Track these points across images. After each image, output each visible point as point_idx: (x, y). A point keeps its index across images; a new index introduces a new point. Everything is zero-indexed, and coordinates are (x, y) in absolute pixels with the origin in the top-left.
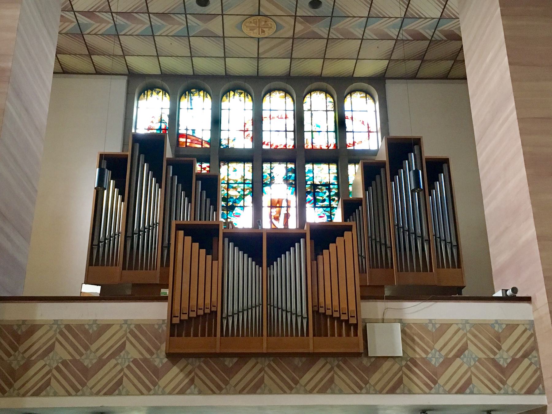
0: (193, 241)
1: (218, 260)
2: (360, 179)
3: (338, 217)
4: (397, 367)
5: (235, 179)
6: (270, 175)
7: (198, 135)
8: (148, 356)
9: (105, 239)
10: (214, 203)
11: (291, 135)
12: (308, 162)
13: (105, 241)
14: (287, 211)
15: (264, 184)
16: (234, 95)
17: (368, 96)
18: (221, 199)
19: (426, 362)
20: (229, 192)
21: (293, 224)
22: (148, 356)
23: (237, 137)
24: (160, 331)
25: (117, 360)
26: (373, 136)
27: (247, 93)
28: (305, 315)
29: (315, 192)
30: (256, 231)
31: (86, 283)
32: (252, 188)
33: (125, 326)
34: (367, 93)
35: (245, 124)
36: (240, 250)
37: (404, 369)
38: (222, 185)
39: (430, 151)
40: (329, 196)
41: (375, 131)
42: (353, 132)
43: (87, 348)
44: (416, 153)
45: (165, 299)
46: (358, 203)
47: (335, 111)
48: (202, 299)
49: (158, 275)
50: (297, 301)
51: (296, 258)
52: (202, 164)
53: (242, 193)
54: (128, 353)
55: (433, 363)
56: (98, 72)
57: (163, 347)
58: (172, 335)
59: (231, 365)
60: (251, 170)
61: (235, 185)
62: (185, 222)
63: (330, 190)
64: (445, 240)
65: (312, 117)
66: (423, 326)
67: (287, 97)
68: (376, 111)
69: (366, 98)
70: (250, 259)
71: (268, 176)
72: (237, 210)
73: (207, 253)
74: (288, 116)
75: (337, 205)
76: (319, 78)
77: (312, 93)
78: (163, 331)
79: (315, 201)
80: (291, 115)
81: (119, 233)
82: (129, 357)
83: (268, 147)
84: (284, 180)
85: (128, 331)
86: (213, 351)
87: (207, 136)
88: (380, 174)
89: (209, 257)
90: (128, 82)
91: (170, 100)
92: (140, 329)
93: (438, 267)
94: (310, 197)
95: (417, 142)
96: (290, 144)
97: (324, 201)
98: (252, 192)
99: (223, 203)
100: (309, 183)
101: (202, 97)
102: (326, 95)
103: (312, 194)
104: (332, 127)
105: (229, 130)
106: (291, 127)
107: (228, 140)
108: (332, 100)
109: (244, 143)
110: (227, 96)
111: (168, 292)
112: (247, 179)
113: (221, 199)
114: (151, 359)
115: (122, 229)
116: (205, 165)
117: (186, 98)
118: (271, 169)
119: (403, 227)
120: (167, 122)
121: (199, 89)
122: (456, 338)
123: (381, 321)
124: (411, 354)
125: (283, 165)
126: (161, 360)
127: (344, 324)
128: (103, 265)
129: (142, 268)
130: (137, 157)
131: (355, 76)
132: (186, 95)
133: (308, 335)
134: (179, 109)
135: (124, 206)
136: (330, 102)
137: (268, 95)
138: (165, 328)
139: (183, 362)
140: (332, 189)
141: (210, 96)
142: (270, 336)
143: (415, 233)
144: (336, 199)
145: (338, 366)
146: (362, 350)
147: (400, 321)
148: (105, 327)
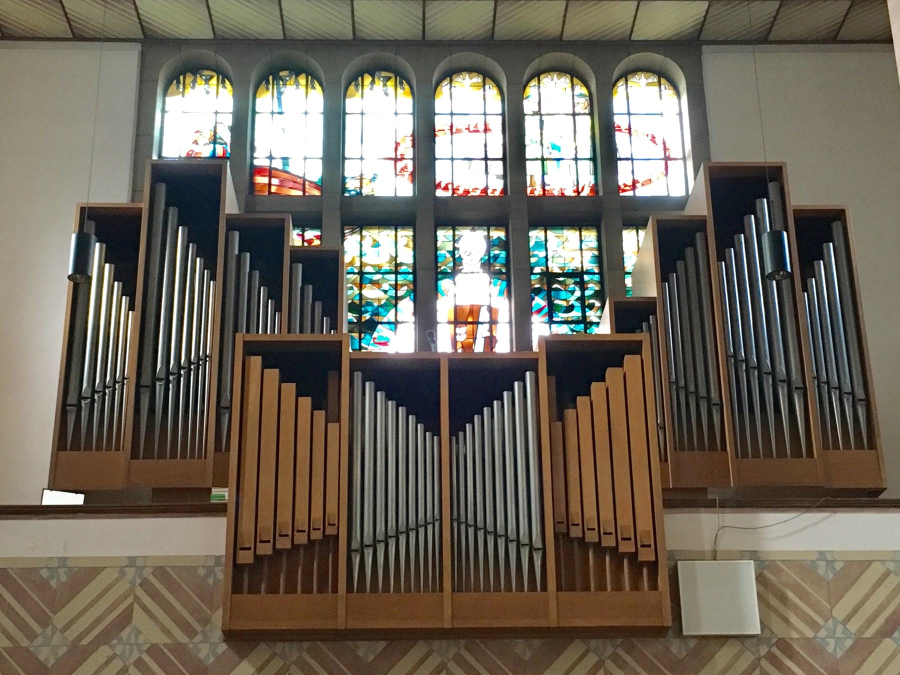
0: (284, 379)
1: (339, 420)
2: (650, 260)
3: (604, 328)
4: (747, 659)
5: (376, 263)
6: (453, 253)
7: (296, 168)
8: (182, 638)
9: (94, 391)
10: (332, 313)
11: (497, 168)
12: (534, 226)
13: (93, 396)
14: (491, 330)
15: (437, 274)
16: (373, 82)
17: (663, 81)
18: (345, 308)
19: (816, 648)
20: (363, 292)
21: (503, 346)
22: (182, 638)
23: (378, 168)
24: (211, 581)
25: (113, 648)
26: (676, 167)
27: (401, 77)
28: (537, 544)
29: (550, 289)
30: (425, 355)
31: (52, 487)
32: (415, 282)
33: (130, 572)
34: (662, 75)
35: (397, 144)
36: (388, 398)
37: (765, 663)
38: (349, 276)
39: (802, 195)
40: (582, 299)
41: (681, 156)
42: (632, 159)
43: (44, 621)
44: (772, 198)
45: (219, 510)
46: (647, 308)
47: (591, 114)
48: (305, 510)
49: (210, 468)
50: (518, 509)
51: (517, 413)
52: (303, 231)
53: (392, 293)
54: (138, 633)
55: (830, 649)
56: (78, 35)
57: (218, 618)
58: (237, 588)
59: (371, 658)
60: (411, 244)
61: (376, 277)
62: (269, 336)
63: (583, 286)
64: (840, 388)
65: (541, 128)
66: (805, 566)
67: (487, 87)
68: (680, 114)
69: (660, 85)
70: (411, 418)
71: (448, 255)
72: (382, 331)
73: (315, 407)
74: (490, 127)
75: (600, 317)
76: (558, 43)
77: (542, 77)
78: (216, 582)
79: (552, 309)
80: (496, 123)
81: (124, 378)
82: (141, 640)
83: (449, 194)
84: (483, 265)
85: (138, 581)
86: (330, 625)
87: (314, 172)
88: (694, 245)
89: (320, 415)
90: (143, 55)
91: (234, 96)
92: (163, 578)
93: (826, 446)
94: (539, 302)
95: (776, 173)
96: (496, 186)
97: (570, 308)
98: (414, 291)
99: (351, 317)
100: (537, 270)
101: (302, 89)
102: (572, 81)
103: (543, 294)
104: (586, 151)
105: (362, 159)
106: (496, 151)
107: (361, 179)
108: (584, 91)
109: (394, 185)
110: (357, 86)
111: (227, 494)
112: (401, 264)
113: (345, 308)
114: (191, 646)
115: (130, 370)
116: (310, 234)
117: (267, 89)
118: (454, 241)
119: (746, 360)
120: (229, 143)
121: (297, 72)
122: (882, 593)
123: (708, 556)
124: (779, 629)
125: (481, 234)
126: (214, 646)
127: (625, 561)
128: (88, 448)
129: (173, 456)
130: (162, 213)
131: (634, 38)
132: (268, 83)
133: (544, 588)
134: (254, 113)
135: (134, 319)
136: (581, 95)
137: (445, 82)
138: (221, 576)
139: (263, 651)
140: (588, 282)
141: (321, 84)
142: (460, 590)
143: (773, 373)
144: (598, 304)
145: (616, 660)
146: (668, 622)
147: (753, 555)
148: (83, 575)
